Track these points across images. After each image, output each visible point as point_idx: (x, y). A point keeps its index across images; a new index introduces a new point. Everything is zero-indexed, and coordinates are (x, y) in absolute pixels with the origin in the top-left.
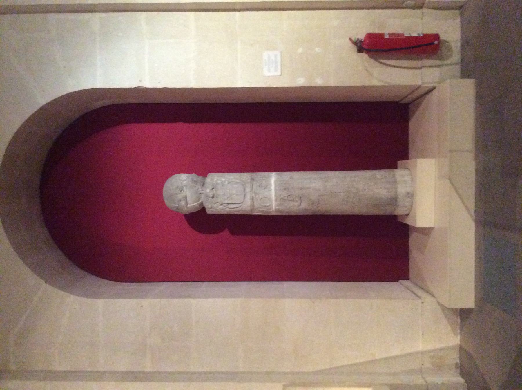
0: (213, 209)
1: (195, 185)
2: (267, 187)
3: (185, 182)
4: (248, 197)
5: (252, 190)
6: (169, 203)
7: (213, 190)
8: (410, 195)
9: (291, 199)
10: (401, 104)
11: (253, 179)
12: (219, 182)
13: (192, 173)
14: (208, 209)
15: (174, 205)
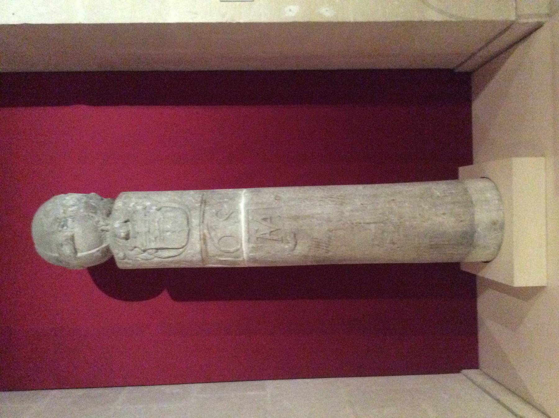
0: (129, 259)
1: (91, 214)
2: (231, 215)
3: (70, 209)
4: (196, 235)
5: (203, 222)
6: (42, 251)
7: (128, 223)
8: (497, 226)
9: (275, 238)
10: (460, 73)
11: (204, 202)
12: (139, 208)
13: (89, 192)
14: (120, 261)
15: (49, 254)
